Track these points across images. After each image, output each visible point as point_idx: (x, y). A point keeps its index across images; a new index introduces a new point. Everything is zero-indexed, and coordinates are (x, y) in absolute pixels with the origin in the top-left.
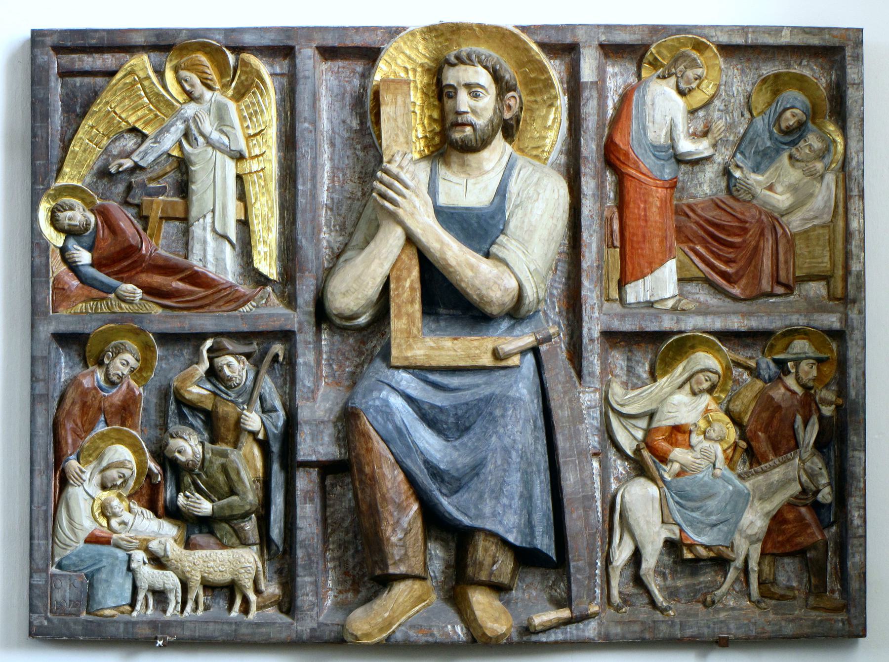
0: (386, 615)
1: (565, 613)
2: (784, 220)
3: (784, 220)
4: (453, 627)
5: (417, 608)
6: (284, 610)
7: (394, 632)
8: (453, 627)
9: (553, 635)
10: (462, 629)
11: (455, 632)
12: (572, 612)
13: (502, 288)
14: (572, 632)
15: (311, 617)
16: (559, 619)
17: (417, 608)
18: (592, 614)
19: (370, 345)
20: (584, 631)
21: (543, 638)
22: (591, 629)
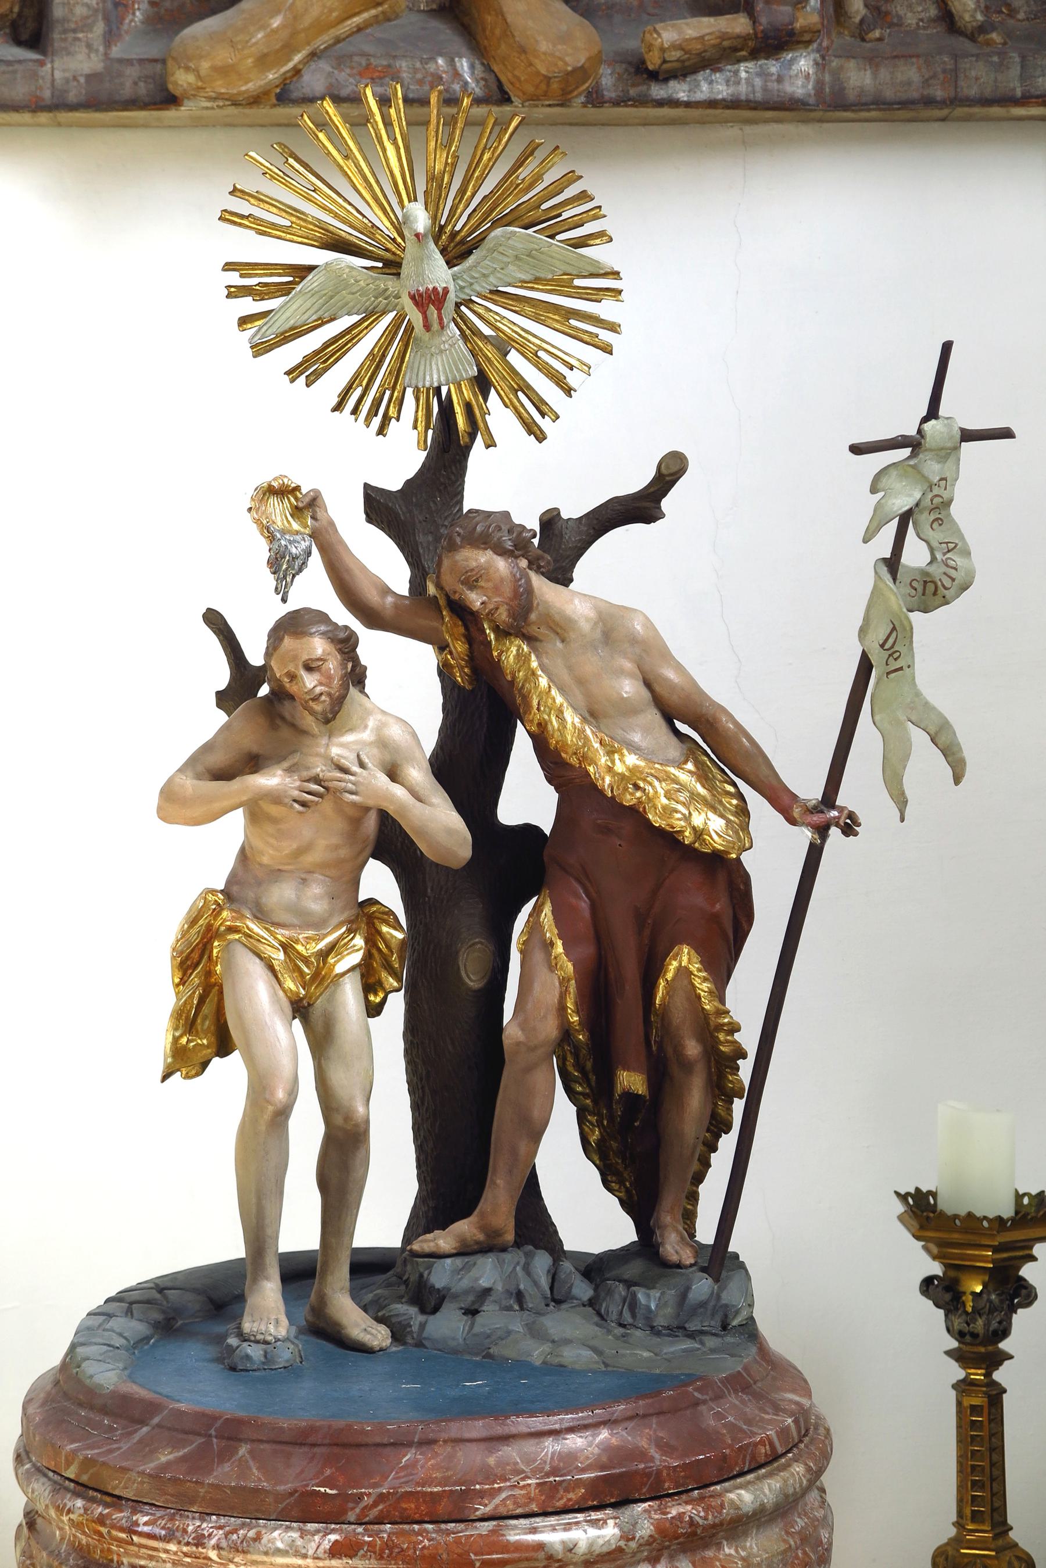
0: (276, 22)
1: (738, 24)
2: (425, 1335)
3: (425, 1335)
4: (451, 62)
5: (357, 20)
6: (25, 37)
7: (297, 72)
8: (451, 62)
9: (705, 87)
10: (472, 67)
11: (457, 75)
12: (754, 21)
13: (493, 13)
14: (745, 77)
15: (89, 46)
16: (724, 36)
17: (357, 20)
18: (804, 31)
19: (220, 895)
20: (780, 79)
21: (680, 90)
22: (800, 70)
